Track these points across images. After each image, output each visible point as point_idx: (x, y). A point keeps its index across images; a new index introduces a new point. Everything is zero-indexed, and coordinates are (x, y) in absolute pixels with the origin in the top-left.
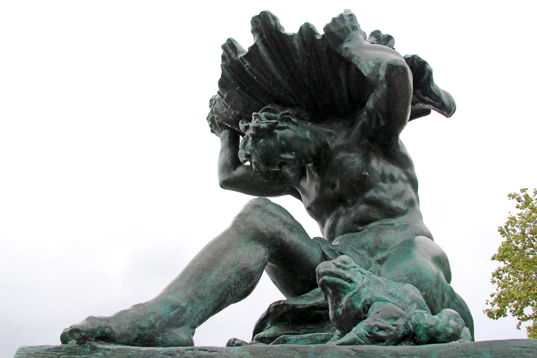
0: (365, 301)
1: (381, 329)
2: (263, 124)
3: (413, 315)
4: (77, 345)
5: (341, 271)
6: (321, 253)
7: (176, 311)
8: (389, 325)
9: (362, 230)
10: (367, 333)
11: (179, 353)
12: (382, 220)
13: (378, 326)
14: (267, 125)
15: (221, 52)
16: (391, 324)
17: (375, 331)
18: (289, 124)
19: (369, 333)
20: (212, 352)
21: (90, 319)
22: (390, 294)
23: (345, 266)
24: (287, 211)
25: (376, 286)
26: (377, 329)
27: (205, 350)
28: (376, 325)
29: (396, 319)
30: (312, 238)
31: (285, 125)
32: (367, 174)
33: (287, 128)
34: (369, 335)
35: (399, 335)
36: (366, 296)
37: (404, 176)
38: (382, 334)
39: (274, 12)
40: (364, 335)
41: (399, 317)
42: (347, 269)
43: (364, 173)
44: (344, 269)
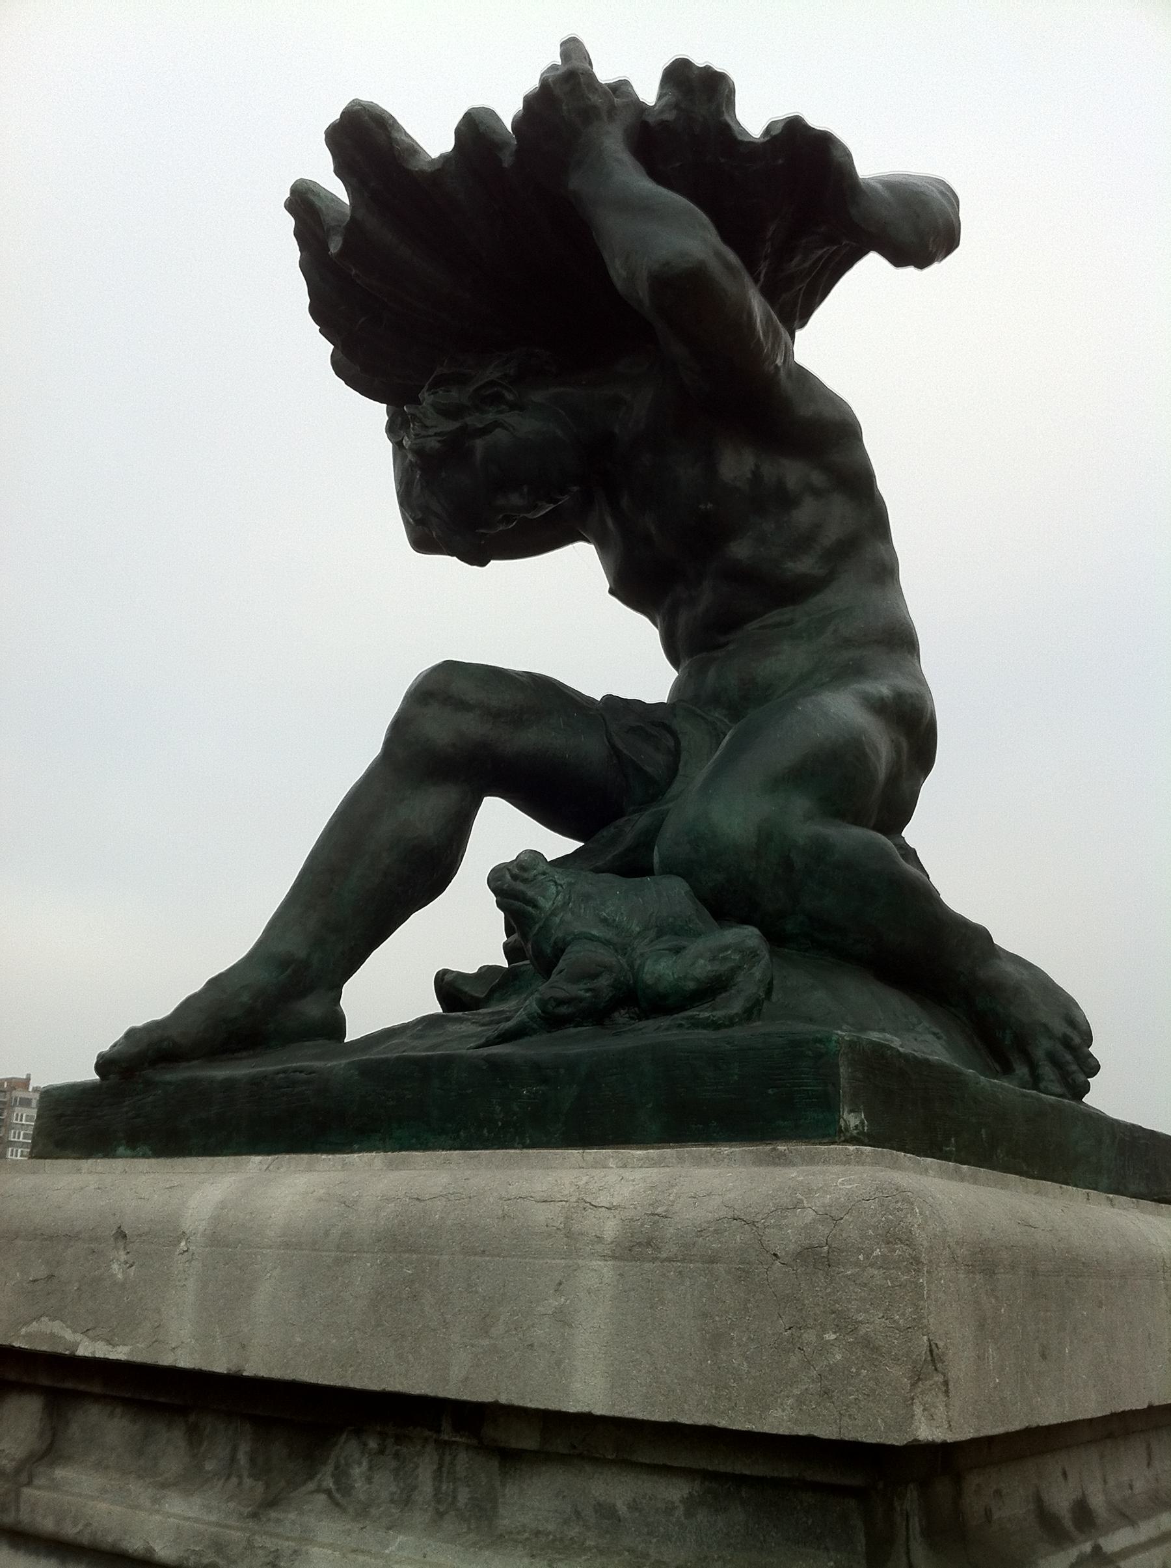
0: (555, 943)
1: (560, 1002)
2: (429, 439)
3: (638, 959)
4: (122, 1081)
5: (521, 886)
6: (607, 744)
7: (289, 971)
8: (579, 992)
9: (727, 644)
10: (540, 1011)
11: (266, 1080)
12: (766, 616)
13: (555, 999)
14: (439, 441)
15: (289, 222)
16: (583, 989)
17: (551, 1008)
18: (501, 412)
19: (543, 1012)
20: (310, 1073)
21: (131, 1034)
22: (604, 921)
23: (526, 875)
24: (954, 192)
25: (583, 906)
26: (554, 1004)
27: (301, 1072)
28: (551, 997)
29: (595, 976)
30: (599, 700)
31: (490, 417)
32: (710, 506)
33: (496, 424)
34: (543, 1015)
35: (603, 1004)
36: (557, 934)
37: (817, 478)
38: (564, 1010)
39: (366, 97)
40: (536, 1015)
41: (601, 973)
42: (530, 880)
43: (702, 507)
44: (525, 881)
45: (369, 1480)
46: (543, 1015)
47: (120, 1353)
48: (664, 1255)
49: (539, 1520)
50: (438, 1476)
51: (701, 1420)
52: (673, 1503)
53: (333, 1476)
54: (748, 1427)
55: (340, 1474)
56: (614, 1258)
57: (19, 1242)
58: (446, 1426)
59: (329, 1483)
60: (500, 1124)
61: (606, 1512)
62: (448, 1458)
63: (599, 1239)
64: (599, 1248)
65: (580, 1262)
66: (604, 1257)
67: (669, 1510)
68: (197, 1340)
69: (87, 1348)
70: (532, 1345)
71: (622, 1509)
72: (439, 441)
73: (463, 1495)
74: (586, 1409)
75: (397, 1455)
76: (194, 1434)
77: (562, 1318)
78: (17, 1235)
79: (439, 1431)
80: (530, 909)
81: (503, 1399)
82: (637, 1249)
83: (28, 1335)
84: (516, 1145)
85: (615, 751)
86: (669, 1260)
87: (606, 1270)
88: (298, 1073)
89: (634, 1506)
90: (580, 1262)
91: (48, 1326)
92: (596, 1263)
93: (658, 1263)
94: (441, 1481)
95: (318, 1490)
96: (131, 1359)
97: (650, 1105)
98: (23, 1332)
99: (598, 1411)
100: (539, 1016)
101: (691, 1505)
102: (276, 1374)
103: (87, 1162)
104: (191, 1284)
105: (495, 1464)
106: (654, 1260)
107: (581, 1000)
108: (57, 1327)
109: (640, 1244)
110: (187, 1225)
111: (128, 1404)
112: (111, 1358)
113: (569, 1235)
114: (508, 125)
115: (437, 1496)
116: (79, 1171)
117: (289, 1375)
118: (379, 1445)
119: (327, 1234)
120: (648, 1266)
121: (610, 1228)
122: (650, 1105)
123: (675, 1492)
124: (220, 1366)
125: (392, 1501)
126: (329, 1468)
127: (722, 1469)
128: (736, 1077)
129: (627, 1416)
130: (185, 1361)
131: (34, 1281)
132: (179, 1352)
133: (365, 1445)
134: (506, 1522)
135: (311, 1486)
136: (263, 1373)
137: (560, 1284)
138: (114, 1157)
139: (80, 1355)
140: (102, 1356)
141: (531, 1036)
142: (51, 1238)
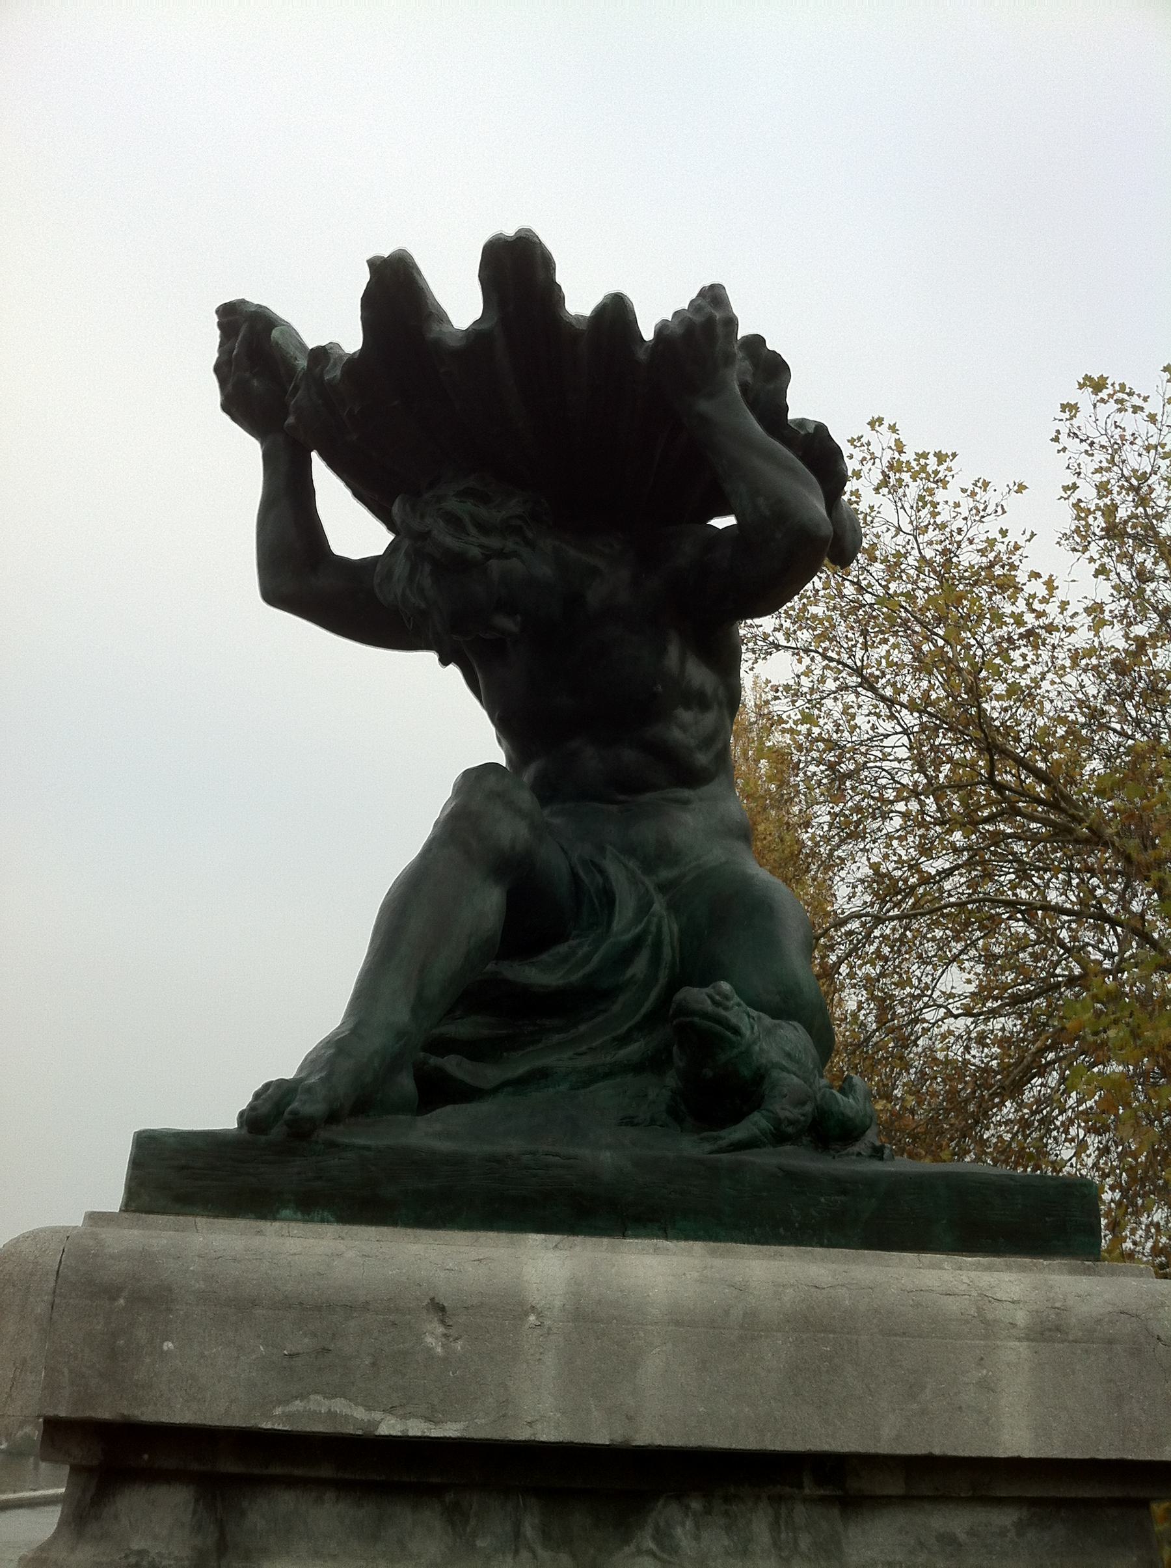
10: (772, 1128)
19: (775, 1129)
29: (803, 1103)
33: (515, 554)
34: (774, 1132)
45: (697, 1538)
46: (774, 1132)
47: (451, 1430)
48: (1071, 1338)
49: (885, 1553)
50: (775, 1526)
51: (1113, 1455)
52: (1006, 1527)
53: (654, 1538)
54: (1149, 1458)
55: (663, 1537)
56: (1028, 1340)
57: (259, 1312)
58: (807, 1481)
59: (651, 1545)
60: (797, 1225)
61: (948, 1541)
62: (783, 1511)
63: (1013, 1325)
64: (1014, 1332)
65: (998, 1343)
66: (1019, 1339)
67: (1003, 1533)
68: (563, 1413)
69: (390, 1427)
70: (960, 1408)
71: (962, 1537)
72: (482, 554)
73: (805, 1541)
74: (1016, 1454)
75: (726, 1513)
76: (455, 1516)
77: (986, 1386)
78: (254, 1303)
79: (800, 1486)
80: (728, 1033)
81: (937, 1451)
82: (1047, 1333)
83: (289, 1416)
84: (814, 1244)
85: (574, 875)
86: (1076, 1341)
87: (1023, 1348)
88: (551, 1157)
89: (972, 1533)
90: (998, 1343)
91: (319, 1404)
92: (1013, 1344)
93: (1066, 1344)
94: (779, 1533)
95: (639, 1552)
96: (467, 1435)
97: (944, 1222)
98: (278, 1411)
99: (1027, 1454)
100: (772, 1133)
101: (1021, 1528)
102: (677, 1441)
103: (271, 1225)
104: (550, 1359)
105: (836, 1512)
106: (1063, 1341)
107: (798, 1121)
108: (340, 1406)
109: (1050, 1330)
110: (535, 1297)
111: (342, 1487)
112: (433, 1435)
113: (985, 1322)
114: (648, 333)
115: (776, 1544)
116: (259, 1233)
117: (693, 1442)
118: (704, 1507)
119: (727, 1313)
120: (1057, 1346)
121: (1021, 1317)
122: (944, 1222)
123: (1006, 1518)
124: (600, 1437)
125: (727, 1553)
126: (649, 1530)
127: (1072, 1494)
128: (1020, 1206)
129: (1050, 1457)
130: (547, 1434)
131: (291, 1356)
132: (539, 1426)
133: (688, 1507)
134: (854, 1558)
135: (632, 1548)
136: (660, 1441)
137: (982, 1359)
138: (275, 1219)
139: (382, 1433)
140: (419, 1434)
141: (760, 1148)
142: (319, 1308)
